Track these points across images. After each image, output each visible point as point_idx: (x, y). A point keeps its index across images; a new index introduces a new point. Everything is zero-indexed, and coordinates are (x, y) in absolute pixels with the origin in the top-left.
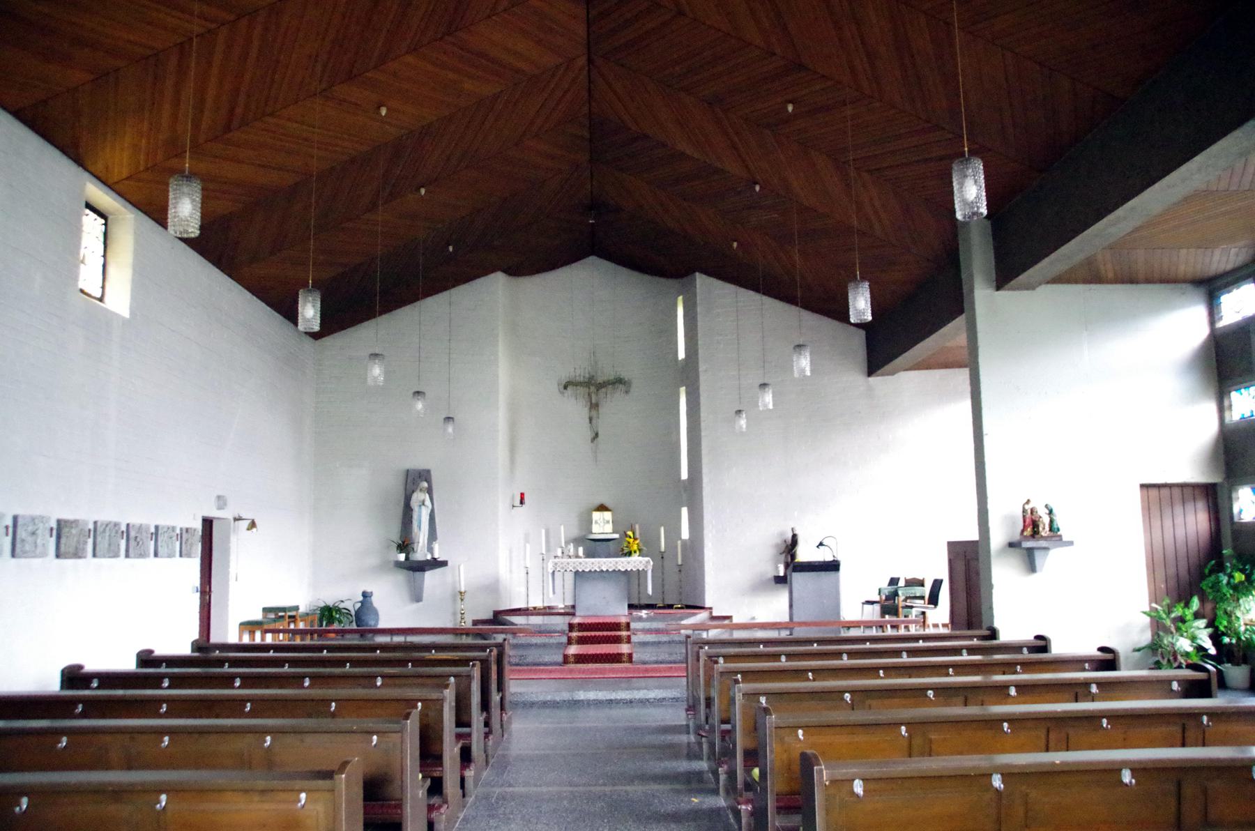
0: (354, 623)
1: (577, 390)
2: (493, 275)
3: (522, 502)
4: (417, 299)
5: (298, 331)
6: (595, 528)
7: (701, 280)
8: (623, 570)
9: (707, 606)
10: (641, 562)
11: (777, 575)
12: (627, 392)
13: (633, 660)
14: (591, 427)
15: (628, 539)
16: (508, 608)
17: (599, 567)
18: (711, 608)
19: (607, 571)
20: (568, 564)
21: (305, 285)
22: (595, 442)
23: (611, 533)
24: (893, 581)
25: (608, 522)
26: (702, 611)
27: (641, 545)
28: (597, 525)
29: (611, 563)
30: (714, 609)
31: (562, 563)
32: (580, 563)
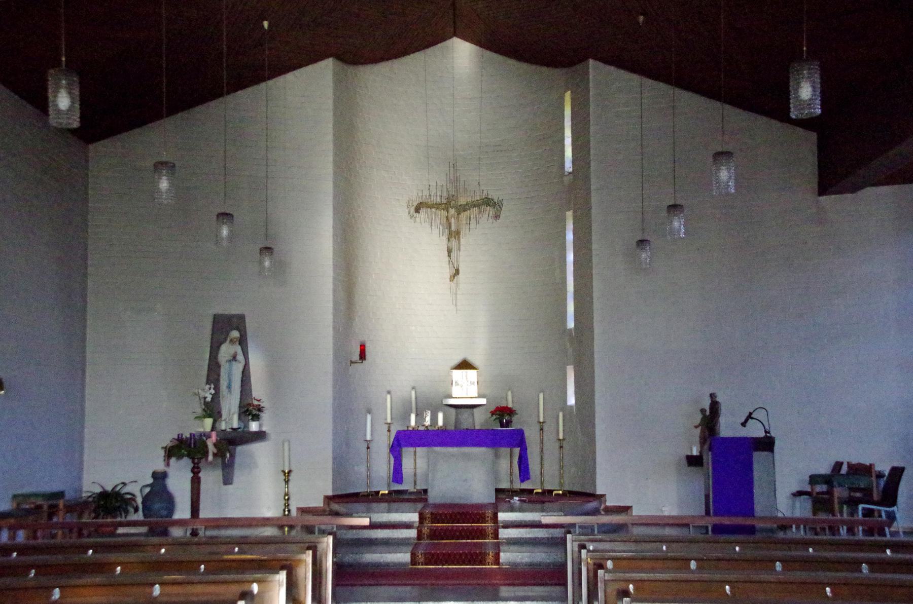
0: (140, 512)
1: (432, 212)
4: (221, 95)
5: (46, 125)
7: (595, 69)
11: (689, 454)
12: (497, 217)
13: (501, 561)
14: (450, 262)
18: (603, 496)
21: (56, 64)
22: (455, 280)
24: (839, 465)
26: (591, 499)
28: (459, 387)
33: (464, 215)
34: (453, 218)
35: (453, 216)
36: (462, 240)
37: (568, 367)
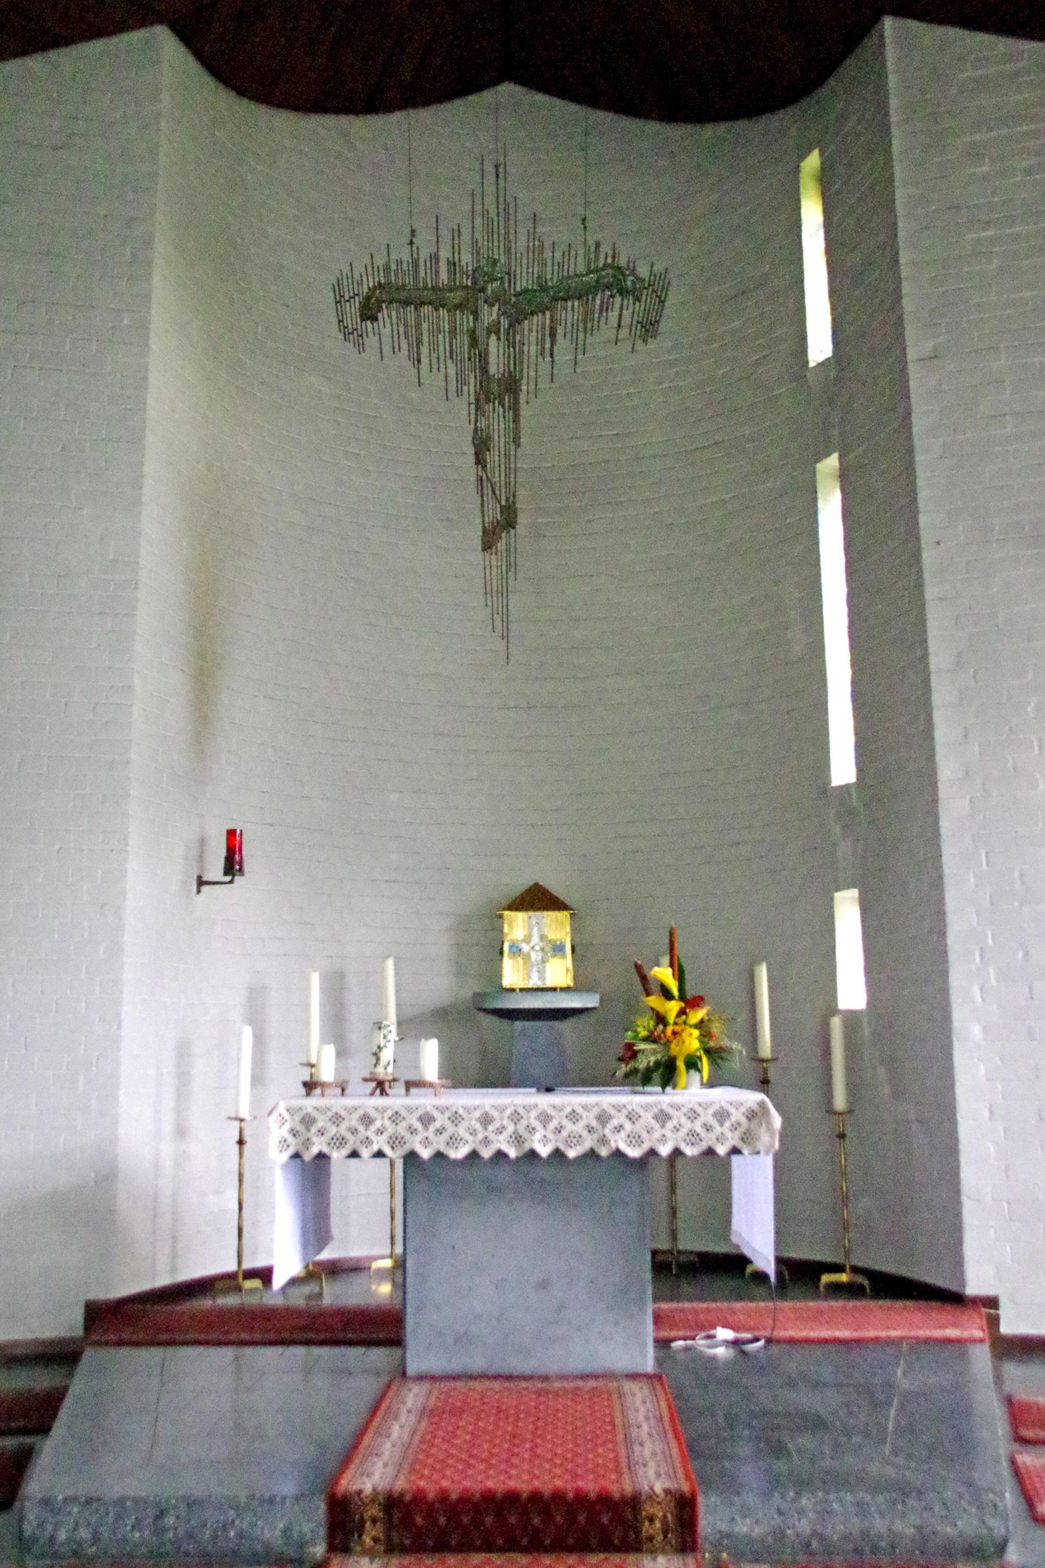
2: (135, 37)
3: (233, 865)
6: (512, 974)
8: (633, 1153)
9: (972, 1289)
10: (722, 1115)
12: (649, 328)
15: (654, 1001)
16: (163, 1280)
17: (518, 1140)
18: (992, 1302)
19: (558, 1154)
20: (367, 1120)
22: (501, 545)
23: (566, 990)
25: (558, 949)
27: (716, 1028)
29: (574, 1117)
30: (1003, 1303)
31: (337, 1119)
32: (427, 1120)
33: (533, 328)
34: (493, 337)
35: (494, 329)
36: (525, 412)
37: (838, 896)
